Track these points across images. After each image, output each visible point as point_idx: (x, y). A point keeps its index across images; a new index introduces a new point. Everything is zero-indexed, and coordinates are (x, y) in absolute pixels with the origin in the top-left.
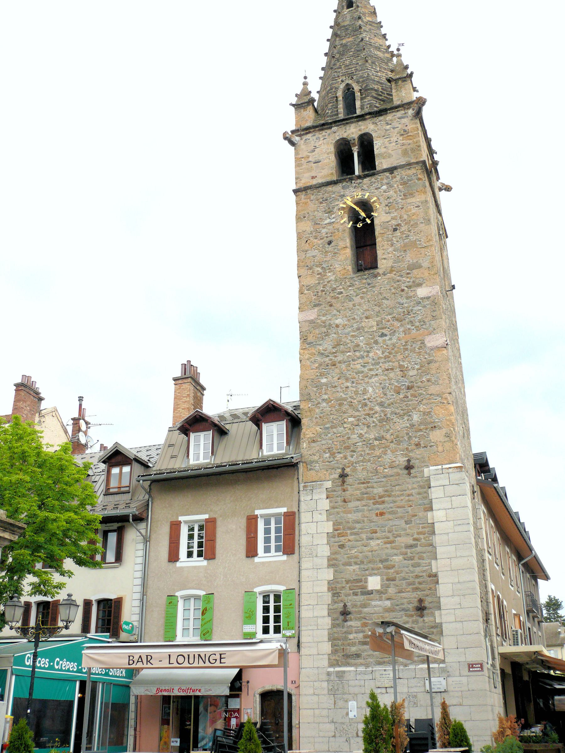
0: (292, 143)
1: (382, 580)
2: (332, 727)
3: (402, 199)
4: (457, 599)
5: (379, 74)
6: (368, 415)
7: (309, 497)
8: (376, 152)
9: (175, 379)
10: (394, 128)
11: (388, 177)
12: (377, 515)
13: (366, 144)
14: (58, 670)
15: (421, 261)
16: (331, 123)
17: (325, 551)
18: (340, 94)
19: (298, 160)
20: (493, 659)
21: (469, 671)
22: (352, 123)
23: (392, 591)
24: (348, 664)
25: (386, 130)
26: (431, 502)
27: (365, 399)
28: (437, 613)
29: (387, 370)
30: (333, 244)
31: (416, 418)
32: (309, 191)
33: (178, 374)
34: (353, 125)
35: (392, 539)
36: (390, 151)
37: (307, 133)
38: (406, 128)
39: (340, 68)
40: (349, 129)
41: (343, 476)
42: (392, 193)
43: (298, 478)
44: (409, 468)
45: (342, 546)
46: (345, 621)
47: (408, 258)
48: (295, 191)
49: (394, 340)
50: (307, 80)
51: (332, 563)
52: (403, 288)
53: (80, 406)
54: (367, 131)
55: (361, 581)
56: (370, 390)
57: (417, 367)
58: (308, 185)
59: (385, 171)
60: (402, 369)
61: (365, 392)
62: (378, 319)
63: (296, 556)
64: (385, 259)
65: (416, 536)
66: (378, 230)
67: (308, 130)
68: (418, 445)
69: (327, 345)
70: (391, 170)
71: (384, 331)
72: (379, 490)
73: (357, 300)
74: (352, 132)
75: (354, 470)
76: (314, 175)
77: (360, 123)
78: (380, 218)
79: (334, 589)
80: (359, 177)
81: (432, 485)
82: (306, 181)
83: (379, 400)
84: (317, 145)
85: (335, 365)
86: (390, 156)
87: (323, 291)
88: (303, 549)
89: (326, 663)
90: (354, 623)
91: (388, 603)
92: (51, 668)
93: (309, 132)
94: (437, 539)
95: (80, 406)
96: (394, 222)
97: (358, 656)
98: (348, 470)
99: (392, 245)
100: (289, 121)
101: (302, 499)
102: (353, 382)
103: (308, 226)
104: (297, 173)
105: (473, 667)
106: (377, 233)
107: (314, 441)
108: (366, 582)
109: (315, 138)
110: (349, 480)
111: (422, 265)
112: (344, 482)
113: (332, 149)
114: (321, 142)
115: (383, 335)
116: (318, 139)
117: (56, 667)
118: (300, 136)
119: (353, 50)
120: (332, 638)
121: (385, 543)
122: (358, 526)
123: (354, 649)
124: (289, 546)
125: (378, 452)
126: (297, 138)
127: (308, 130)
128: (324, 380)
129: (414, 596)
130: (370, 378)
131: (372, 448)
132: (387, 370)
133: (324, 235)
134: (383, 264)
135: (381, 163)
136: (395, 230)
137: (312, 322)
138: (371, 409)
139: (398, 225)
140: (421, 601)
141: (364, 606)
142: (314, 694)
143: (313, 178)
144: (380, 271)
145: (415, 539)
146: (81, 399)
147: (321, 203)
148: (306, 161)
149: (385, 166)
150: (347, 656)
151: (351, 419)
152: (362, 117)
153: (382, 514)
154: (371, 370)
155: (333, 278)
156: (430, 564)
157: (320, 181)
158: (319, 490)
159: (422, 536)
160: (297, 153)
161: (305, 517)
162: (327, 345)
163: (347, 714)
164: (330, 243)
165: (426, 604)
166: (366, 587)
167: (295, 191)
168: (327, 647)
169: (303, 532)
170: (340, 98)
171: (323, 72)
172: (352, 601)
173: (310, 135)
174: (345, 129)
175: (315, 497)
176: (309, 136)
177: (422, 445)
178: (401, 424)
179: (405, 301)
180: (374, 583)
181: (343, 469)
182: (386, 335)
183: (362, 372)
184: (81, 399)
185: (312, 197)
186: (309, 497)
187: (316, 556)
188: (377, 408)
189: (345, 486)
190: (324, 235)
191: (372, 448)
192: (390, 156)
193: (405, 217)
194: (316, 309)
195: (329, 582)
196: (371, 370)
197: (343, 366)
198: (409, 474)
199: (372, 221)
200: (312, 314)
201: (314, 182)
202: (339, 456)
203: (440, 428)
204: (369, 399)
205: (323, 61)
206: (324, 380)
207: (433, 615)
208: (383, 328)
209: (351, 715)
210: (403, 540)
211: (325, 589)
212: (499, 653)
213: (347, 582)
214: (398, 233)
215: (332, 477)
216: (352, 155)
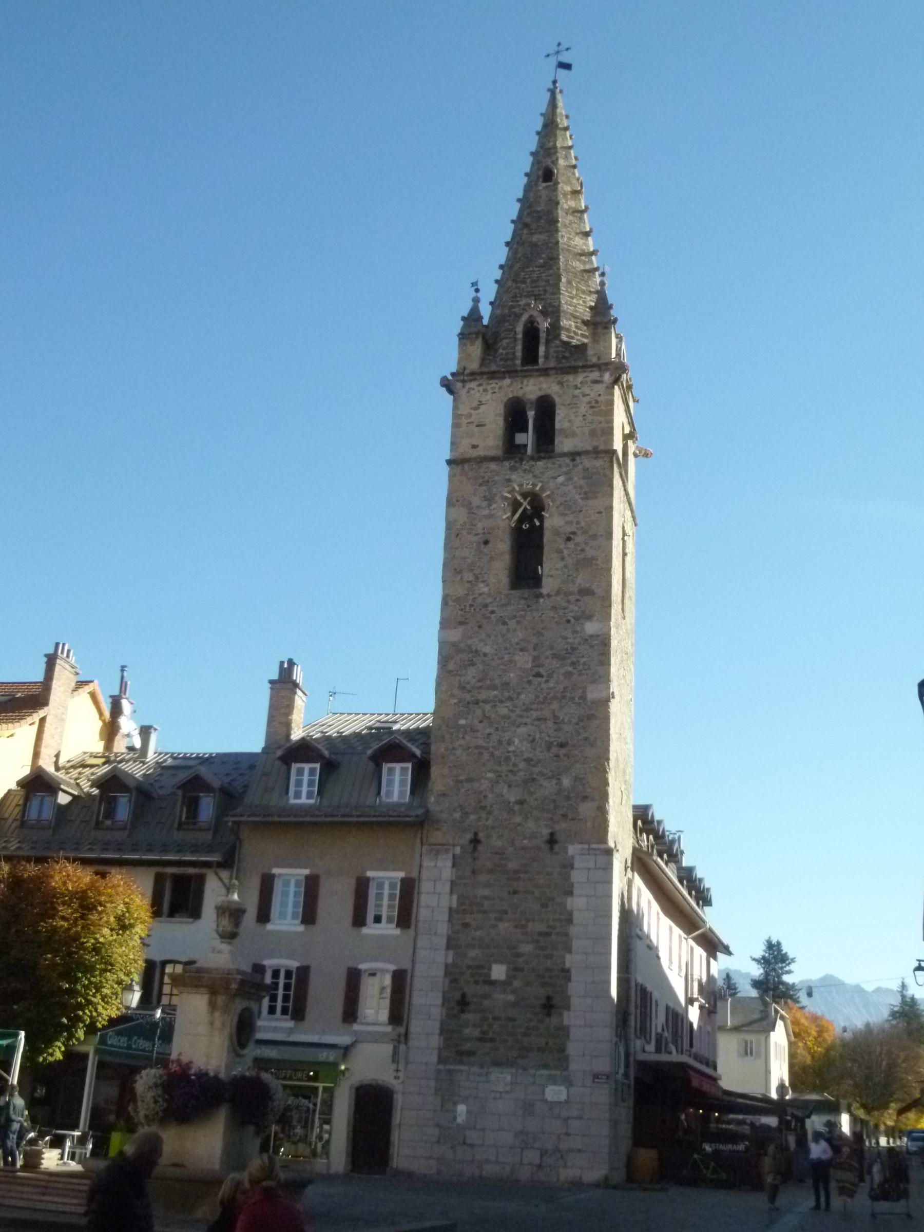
0: (451, 391)
1: (508, 970)
2: (436, 1132)
3: (582, 499)
4: (589, 1001)
5: (575, 301)
6: (511, 771)
7: (432, 864)
8: (558, 425)
9: (271, 682)
10: (584, 395)
11: (568, 465)
12: (509, 893)
13: (546, 408)
14: (135, 1050)
15: (594, 587)
16: (504, 372)
17: (443, 928)
18: (520, 329)
19: (456, 416)
20: (627, 1066)
21: (594, 1082)
22: (531, 376)
23: (517, 984)
24: (461, 1062)
25: (575, 397)
26: (572, 885)
27: (509, 752)
28: (565, 1014)
29: (539, 719)
30: (490, 545)
31: (566, 782)
32: (466, 466)
33: (275, 676)
34: (532, 381)
35: (524, 922)
36: (575, 428)
37: (471, 381)
38: (599, 399)
39: (524, 282)
40: (527, 385)
41: (475, 841)
42: (570, 487)
43: (422, 838)
44: (552, 841)
45: (466, 925)
46: (463, 1012)
47: (579, 580)
48: (449, 462)
49: (551, 684)
50: (479, 295)
51: (451, 944)
52: (569, 618)
53: (122, 678)
54: (549, 392)
55: (482, 967)
56: (516, 741)
57: (574, 721)
58: (467, 456)
59: (565, 455)
60: (557, 721)
61: (510, 742)
62: (535, 653)
63: (411, 931)
64: (552, 576)
65: (551, 923)
66: (547, 536)
67: (473, 375)
68: (564, 816)
69: (471, 675)
70: (574, 455)
71: (542, 670)
72: (512, 865)
73: (512, 624)
74: (531, 389)
75: (489, 837)
76: (475, 443)
77: (542, 379)
78: (552, 521)
79: (451, 973)
80: (532, 458)
81: (576, 865)
82: (465, 449)
83: (526, 755)
84: (483, 400)
85: (477, 703)
86: (574, 434)
87: (471, 605)
88: (420, 925)
89: (434, 1059)
90: (470, 1017)
91: (511, 998)
92: (129, 1047)
93: (475, 380)
94: (573, 930)
95: (122, 678)
96: (569, 529)
97: (471, 1053)
98: (481, 836)
99: (563, 559)
100: (448, 360)
101: (425, 864)
102: (497, 729)
103: (461, 515)
104: (453, 435)
105: (598, 1078)
106: (545, 540)
107: (444, 795)
108: (490, 969)
109: (481, 388)
110: (481, 848)
111: (596, 591)
112: (475, 849)
113: (501, 409)
114: (489, 396)
115: (538, 675)
116: (485, 390)
117: (134, 1046)
118: (464, 381)
119: (544, 256)
120: (443, 1030)
121: (516, 927)
122: (486, 903)
123: (468, 1046)
124: (405, 918)
125: (518, 819)
126: (459, 385)
127: (473, 375)
128: (462, 722)
129: (542, 992)
130: (518, 726)
131: (511, 811)
132: (539, 719)
133: (480, 531)
134: (548, 585)
135: (563, 444)
136: (569, 539)
137: (454, 645)
138: (515, 765)
139: (574, 533)
140: (549, 998)
141: (486, 996)
142: (419, 1094)
143: (474, 447)
144: (544, 591)
145: (549, 927)
146: (123, 669)
147: (481, 485)
148: (467, 421)
149: (566, 450)
150: (460, 1053)
151: (490, 775)
152: (545, 372)
153: (515, 892)
154: (521, 716)
155: (486, 590)
156: (563, 957)
157: (480, 452)
158: (444, 856)
159: (558, 924)
160: (455, 408)
161: (426, 886)
162: (471, 675)
163: (455, 1118)
164: (486, 543)
165: (555, 1002)
166: (489, 975)
167: (449, 462)
168: (436, 1041)
169: (422, 904)
170: (520, 336)
171: (501, 271)
172: (470, 990)
173: (476, 383)
174: (522, 383)
175: (440, 864)
176: (473, 385)
177: (570, 817)
178: (548, 788)
179: (570, 635)
180: (499, 972)
181: (476, 834)
182: (542, 676)
183: (509, 718)
184: (123, 669)
185: (470, 474)
186: (432, 864)
187: (435, 934)
188: (522, 765)
189: (477, 854)
190: (480, 531)
191: (511, 811)
192: (574, 434)
193: (583, 524)
194: (460, 629)
195: (447, 966)
196: (521, 716)
197: (487, 707)
198: (552, 849)
199: (542, 522)
200: (455, 635)
201: (474, 453)
202: (472, 817)
203: (593, 800)
204: (514, 752)
205: (502, 255)
206: (462, 722)
207: (561, 1015)
208: (538, 666)
209: (459, 1120)
210: (536, 927)
211: (442, 973)
212: (635, 1060)
213: (469, 967)
214: (571, 545)
215: (462, 842)
216: (527, 422)
